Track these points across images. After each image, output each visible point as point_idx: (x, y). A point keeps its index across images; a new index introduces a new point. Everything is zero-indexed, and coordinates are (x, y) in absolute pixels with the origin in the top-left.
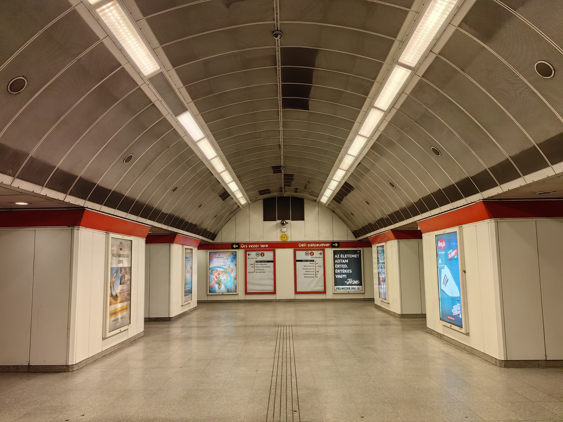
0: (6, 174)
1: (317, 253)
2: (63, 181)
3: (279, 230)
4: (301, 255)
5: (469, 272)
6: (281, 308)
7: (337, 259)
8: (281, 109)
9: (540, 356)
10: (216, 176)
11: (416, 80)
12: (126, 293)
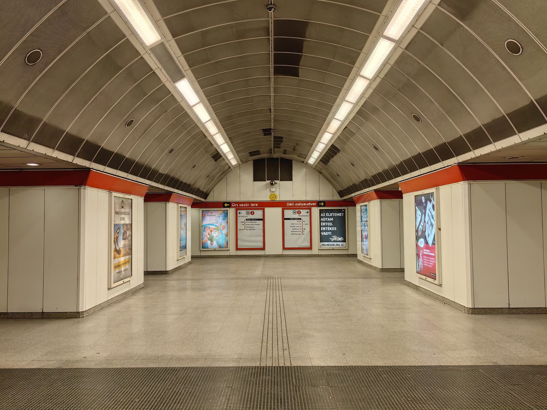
0: (22, 138)
1: (304, 212)
2: (72, 144)
3: (268, 190)
4: (289, 213)
6: (270, 263)
7: (323, 217)
8: (272, 76)
10: (209, 138)
11: (399, 52)
12: (127, 248)
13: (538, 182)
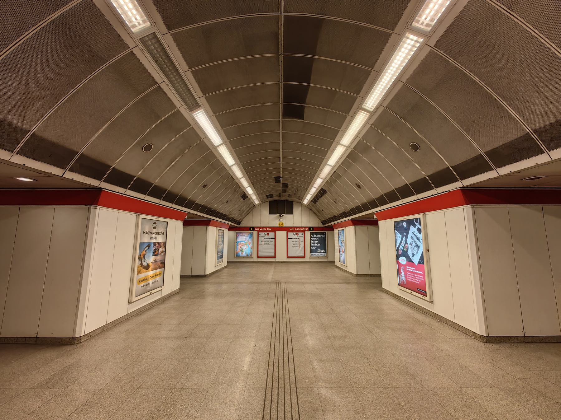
4: (291, 235)
5: (449, 250)
6: (280, 268)
9: (367, 273)
10: (237, 181)
13: (539, 207)
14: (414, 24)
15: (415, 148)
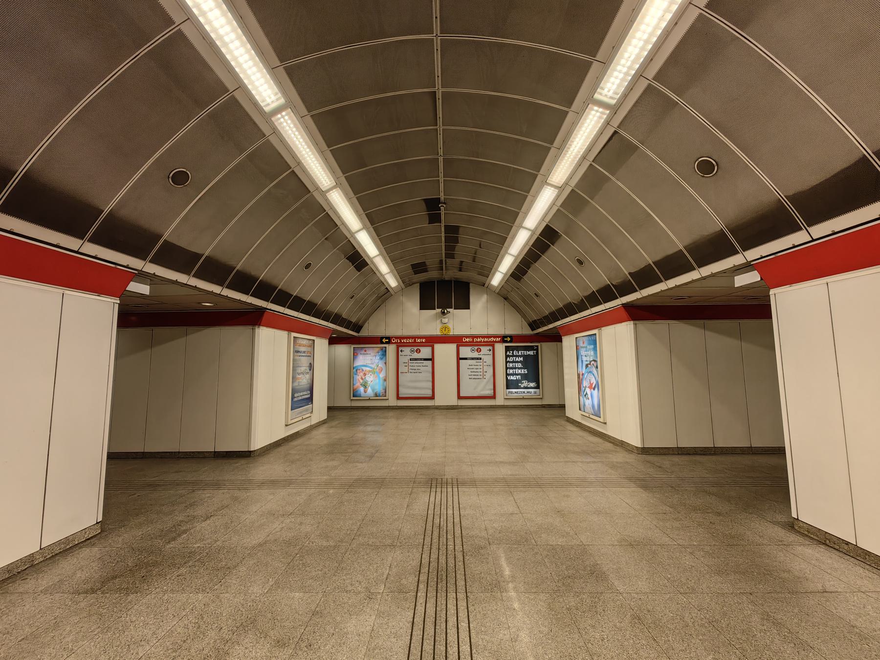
1: (485, 350)
2: (214, 270)
3: (438, 321)
4: (465, 351)
6: (443, 423)
7: (509, 356)
13: (702, 322)
14: (597, 96)
15: (706, 168)
